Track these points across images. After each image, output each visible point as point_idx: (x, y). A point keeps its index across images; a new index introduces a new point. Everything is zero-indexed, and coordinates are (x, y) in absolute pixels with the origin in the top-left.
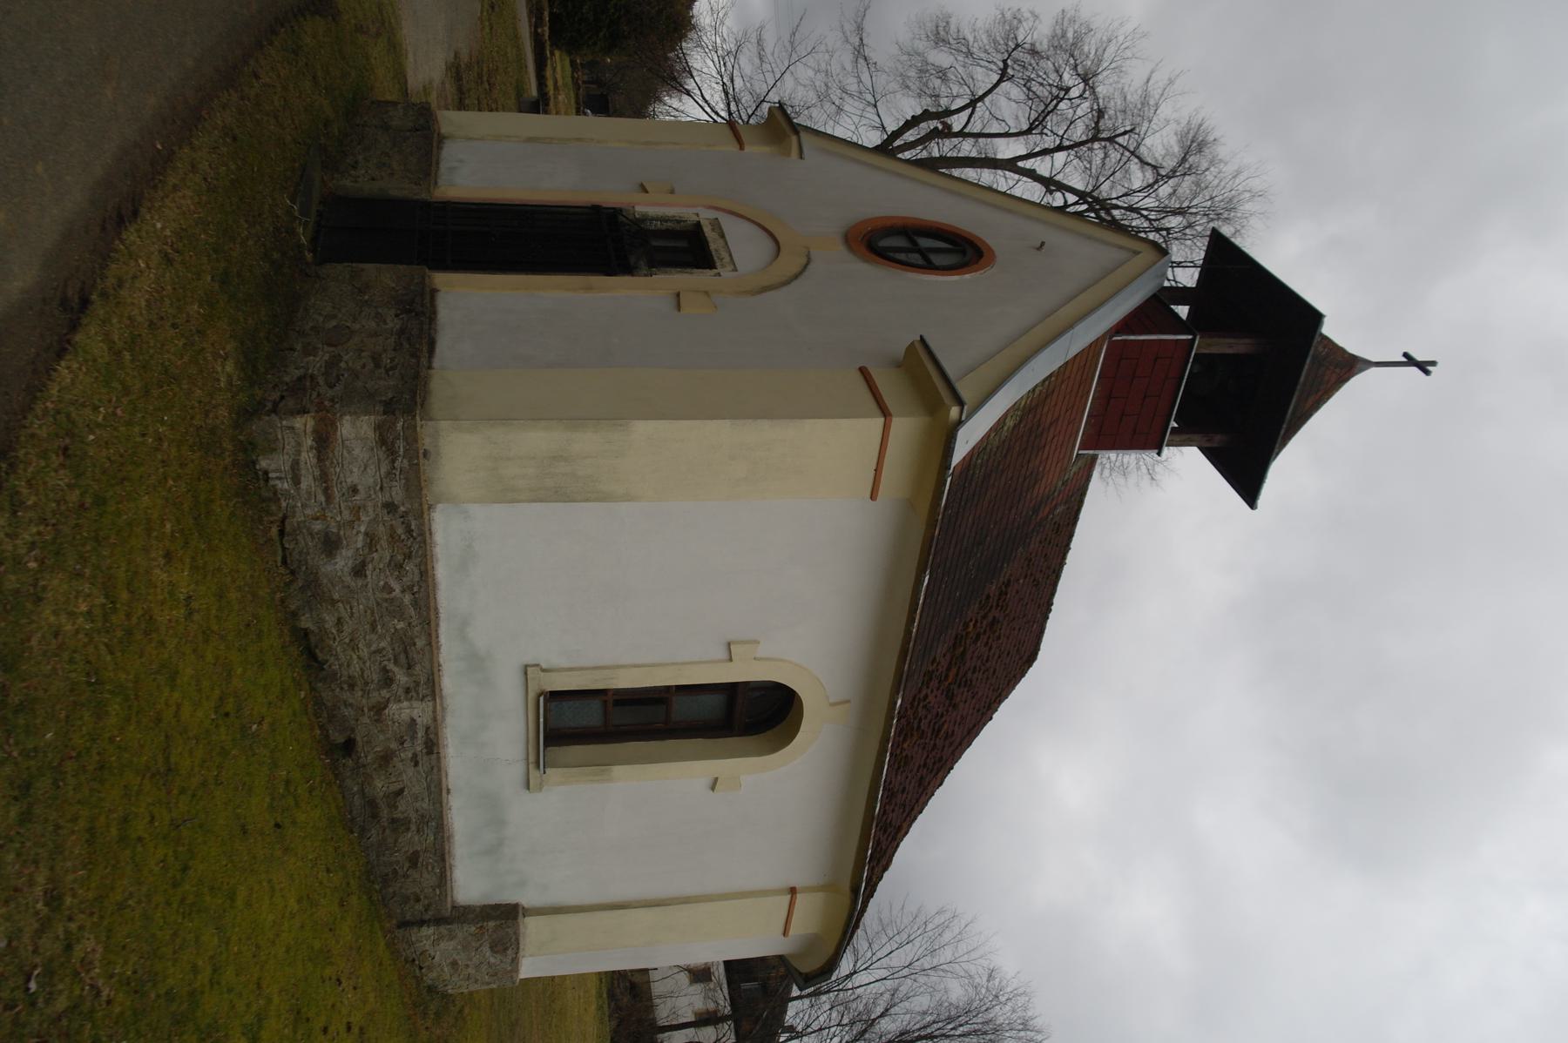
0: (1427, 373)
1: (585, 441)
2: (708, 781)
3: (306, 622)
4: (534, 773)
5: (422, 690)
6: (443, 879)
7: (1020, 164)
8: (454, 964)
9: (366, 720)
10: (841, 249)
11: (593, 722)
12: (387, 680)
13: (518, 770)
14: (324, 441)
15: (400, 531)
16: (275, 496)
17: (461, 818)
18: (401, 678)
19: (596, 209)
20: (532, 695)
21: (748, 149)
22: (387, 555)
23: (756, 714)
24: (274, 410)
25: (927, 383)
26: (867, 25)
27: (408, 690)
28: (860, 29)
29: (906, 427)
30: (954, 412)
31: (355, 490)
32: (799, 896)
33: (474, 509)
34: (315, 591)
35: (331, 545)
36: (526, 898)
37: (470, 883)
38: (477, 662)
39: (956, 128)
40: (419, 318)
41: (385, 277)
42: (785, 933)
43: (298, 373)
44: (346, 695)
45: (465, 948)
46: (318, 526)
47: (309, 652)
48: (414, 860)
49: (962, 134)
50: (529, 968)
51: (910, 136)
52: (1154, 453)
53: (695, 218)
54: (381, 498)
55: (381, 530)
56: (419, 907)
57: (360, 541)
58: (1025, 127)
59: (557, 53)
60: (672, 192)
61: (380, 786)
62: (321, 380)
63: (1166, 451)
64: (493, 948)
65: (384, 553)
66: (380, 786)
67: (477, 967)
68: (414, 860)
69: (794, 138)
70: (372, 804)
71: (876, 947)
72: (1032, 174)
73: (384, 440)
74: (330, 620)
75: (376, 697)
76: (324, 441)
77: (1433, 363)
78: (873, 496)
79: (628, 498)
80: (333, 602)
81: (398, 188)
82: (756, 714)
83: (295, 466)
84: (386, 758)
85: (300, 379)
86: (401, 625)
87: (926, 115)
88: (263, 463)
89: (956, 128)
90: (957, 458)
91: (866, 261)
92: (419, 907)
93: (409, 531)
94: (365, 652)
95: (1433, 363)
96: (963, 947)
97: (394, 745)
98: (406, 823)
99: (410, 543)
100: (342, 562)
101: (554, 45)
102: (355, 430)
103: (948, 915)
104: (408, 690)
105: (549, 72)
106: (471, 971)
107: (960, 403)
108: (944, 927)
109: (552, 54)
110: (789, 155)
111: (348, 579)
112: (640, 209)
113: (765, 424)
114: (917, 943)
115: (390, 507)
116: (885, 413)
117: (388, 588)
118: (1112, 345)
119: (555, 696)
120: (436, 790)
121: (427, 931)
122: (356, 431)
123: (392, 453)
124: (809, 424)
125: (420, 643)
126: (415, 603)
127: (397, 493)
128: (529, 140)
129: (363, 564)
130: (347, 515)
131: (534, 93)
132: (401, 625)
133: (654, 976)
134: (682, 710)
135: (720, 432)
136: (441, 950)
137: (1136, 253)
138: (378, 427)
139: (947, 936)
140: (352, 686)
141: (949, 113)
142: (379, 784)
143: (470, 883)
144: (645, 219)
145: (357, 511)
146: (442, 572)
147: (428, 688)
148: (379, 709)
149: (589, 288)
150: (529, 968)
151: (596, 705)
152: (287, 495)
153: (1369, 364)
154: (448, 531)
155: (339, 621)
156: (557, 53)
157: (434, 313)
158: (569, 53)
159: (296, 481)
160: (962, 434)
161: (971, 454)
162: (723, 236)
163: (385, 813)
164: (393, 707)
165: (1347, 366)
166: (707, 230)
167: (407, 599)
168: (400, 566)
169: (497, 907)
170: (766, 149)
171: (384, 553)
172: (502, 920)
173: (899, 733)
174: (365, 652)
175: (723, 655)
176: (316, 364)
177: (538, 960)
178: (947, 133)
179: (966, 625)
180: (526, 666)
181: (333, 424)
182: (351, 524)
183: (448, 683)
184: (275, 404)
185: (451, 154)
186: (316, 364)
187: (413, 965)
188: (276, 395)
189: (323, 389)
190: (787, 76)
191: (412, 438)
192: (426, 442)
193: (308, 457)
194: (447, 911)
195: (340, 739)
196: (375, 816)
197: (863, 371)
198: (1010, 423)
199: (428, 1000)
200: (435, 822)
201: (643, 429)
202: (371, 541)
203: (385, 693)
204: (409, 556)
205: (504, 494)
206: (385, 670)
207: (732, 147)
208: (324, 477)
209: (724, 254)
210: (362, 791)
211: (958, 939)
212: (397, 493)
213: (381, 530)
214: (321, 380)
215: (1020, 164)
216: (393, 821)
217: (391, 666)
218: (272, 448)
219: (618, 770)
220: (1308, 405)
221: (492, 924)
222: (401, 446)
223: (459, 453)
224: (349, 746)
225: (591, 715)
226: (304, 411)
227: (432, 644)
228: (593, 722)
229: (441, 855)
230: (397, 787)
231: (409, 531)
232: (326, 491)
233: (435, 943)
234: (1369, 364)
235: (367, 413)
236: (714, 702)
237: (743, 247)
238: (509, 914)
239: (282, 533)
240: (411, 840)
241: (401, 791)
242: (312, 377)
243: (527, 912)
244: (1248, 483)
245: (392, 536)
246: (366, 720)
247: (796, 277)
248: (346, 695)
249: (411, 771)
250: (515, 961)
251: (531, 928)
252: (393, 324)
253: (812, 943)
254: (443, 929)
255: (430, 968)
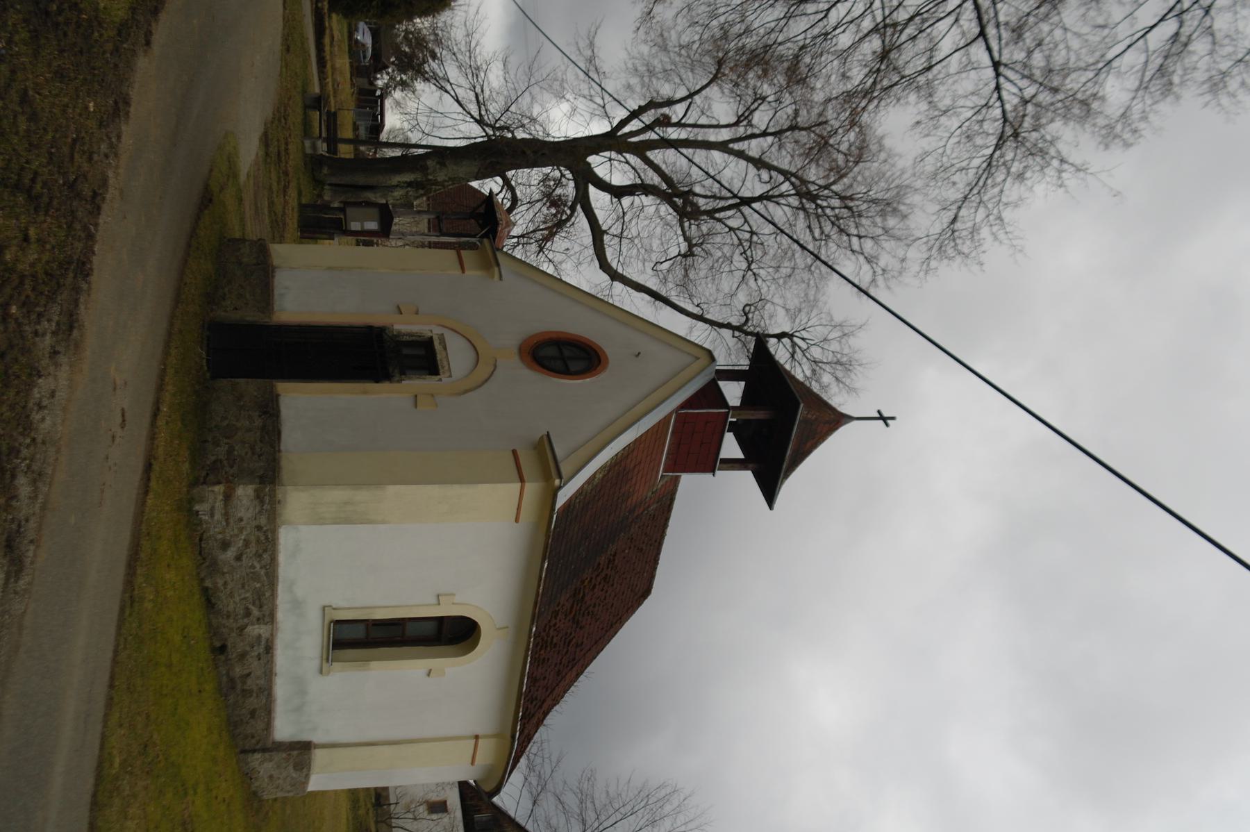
0: (887, 425)
1: (362, 495)
2: (426, 671)
3: (208, 583)
4: (325, 664)
5: (267, 619)
6: (268, 726)
7: (731, 145)
8: (271, 777)
9: (234, 635)
10: (516, 359)
11: (361, 638)
12: (248, 613)
13: (315, 663)
14: (228, 497)
15: (262, 538)
16: (201, 523)
17: (281, 689)
18: (256, 612)
19: (370, 328)
20: (327, 622)
21: (467, 272)
22: (254, 551)
23: (456, 633)
24: (204, 483)
25: (545, 461)
26: (597, 42)
27: (258, 619)
28: (591, 45)
29: (533, 488)
30: (557, 482)
31: (241, 520)
32: (480, 741)
33: (303, 528)
34: (214, 567)
35: (225, 545)
36: (316, 738)
37: (284, 729)
38: (297, 605)
39: (674, 120)
40: (270, 411)
41: (250, 387)
42: (473, 763)
43: (213, 458)
44: (224, 621)
45: (278, 767)
46: (220, 536)
47: (209, 601)
48: (253, 713)
49: (679, 124)
50: (315, 783)
51: (635, 125)
52: (709, 476)
53: (429, 334)
54: (254, 523)
55: (253, 538)
56: (253, 741)
57: (241, 543)
58: (733, 120)
59: (334, 16)
60: (417, 313)
61: (238, 671)
62: (225, 463)
63: (718, 473)
64: (295, 768)
65: (253, 549)
66: (238, 671)
67: (285, 779)
68: (253, 713)
69: (496, 269)
70: (232, 680)
71: (603, 818)
72: (741, 155)
73: (259, 497)
74: (220, 582)
75: (241, 622)
76: (228, 497)
77: (893, 418)
78: (517, 520)
79: (383, 522)
80: (224, 574)
81: (250, 315)
82: (456, 633)
83: (213, 508)
84: (243, 656)
85: (215, 462)
86: (258, 585)
87: (652, 105)
88: (197, 507)
89: (674, 120)
90: (563, 497)
91: (530, 367)
92: (253, 741)
93: (267, 538)
94: (237, 599)
95: (893, 418)
96: (681, 819)
97: (248, 648)
98: (251, 692)
99: (267, 544)
100: (231, 553)
101: (332, 8)
102: (245, 492)
103: (668, 790)
104: (258, 619)
105: (327, 40)
106: (281, 781)
107: (560, 477)
108: (666, 799)
109: (330, 17)
110: (493, 277)
111: (233, 562)
112: (396, 327)
113: (456, 487)
114: (640, 814)
115: (259, 528)
116: (522, 480)
117: (253, 567)
118: (678, 416)
119: (338, 622)
120: (269, 674)
121: (258, 756)
122: (245, 492)
123: (262, 502)
124: (480, 486)
125: (267, 594)
126: (267, 574)
127: (263, 521)
128: (330, 268)
129: (241, 555)
130: (236, 531)
131: (317, 90)
132: (258, 585)
133: (391, 791)
134: (411, 630)
135: (433, 491)
136: (263, 766)
137: (698, 358)
138: (256, 491)
139: (668, 808)
140: (228, 617)
141: (670, 102)
142: (237, 670)
143: (284, 729)
144: (400, 334)
145: (241, 530)
146: (282, 558)
147: (269, 618)
148: (242, 629)
149: (365, 392)
150: (315, 783)
151: (362, 627)
152: (207, 523)
153: (850, 418)
154: (286, 538)
155: (225, 584)
156: (334, 16)
157: (279, 411)
158: (346, 16)
159: (212, 515)
160: (560, 494)
161: (570, 500)
162: (445, 349)
163: (239, 686)
164: (250, 628)
165: (837, 419)
166: (436, 343)
167: (263, 572)
168: (260, 556)
169: (299, 743)
170: (479, 273)
171: (253, 549)
172: (301, 751)
173: (536, 645)
174: (237, 599)
175: (434, 601)
176: (222, 451)
177: (325, 777)
178: (665, 122)
179: (583, 582)
180: (324, 608)
181: (234, 489)
182: (237, 536)
183: (280, 615)
184: (205, 478)
185: (282, 281)
186: (222, 451)
187: (248, 776)
188: (204, 473)
189: (228, 469)
190: (527, 94)
191: (273, 494)
192: (279, 496)
193: (219, 505)
194: (269, 745)
195: (218, 644)
196: (233, 688)
197: (514, 452)
198: (600, 476)
199: (253, 801)
200: (267, 692)
201: (392, 489)
202: (247, 543)
203: (246, 620)
204: (265, 551)
205: (320, 521)
206: (247, 609)
207: (458, 272)
208: (226, 515)
209: (445, 363)
210: (228, 674)
211: (678, 811)
212: (263, 521)
213: (253, 538)
214: (225, 463)
215: (731, 145)
216: (243, 691)
217: (251, 606)
218: (202, 500)
219: (374, 664)
220: (809, 444)
221: (295, 753)
222: (267, 499)
223: (295, 501)
224: (223, 649)
225: (359, 633)
226: (219, 483)
227: (274, 595)
228: (361, 638)
229: (269, 711)
230: (246, 672)
231: (267, 538)
232: (227, 520)
233: (261, 763)
234: (850, 418)
235: (251, 483)
236: (432, 625)
237: (456, 356)
238: (305, 748)
239: (201, 540)
240: (252, 702)
241: (249, 675)
242: (221, 461)
243: (317, 746)
244: (770, 494)
245: (258, 541)
246: (234, 635)
247: (486, 381)
248: (224, 621)
249: (256, 663)
250: (307, 776)
251: (318, 756)
252: (258, 422)
253: (490, 770)
254: (267, 755)
255: (256, 779)
